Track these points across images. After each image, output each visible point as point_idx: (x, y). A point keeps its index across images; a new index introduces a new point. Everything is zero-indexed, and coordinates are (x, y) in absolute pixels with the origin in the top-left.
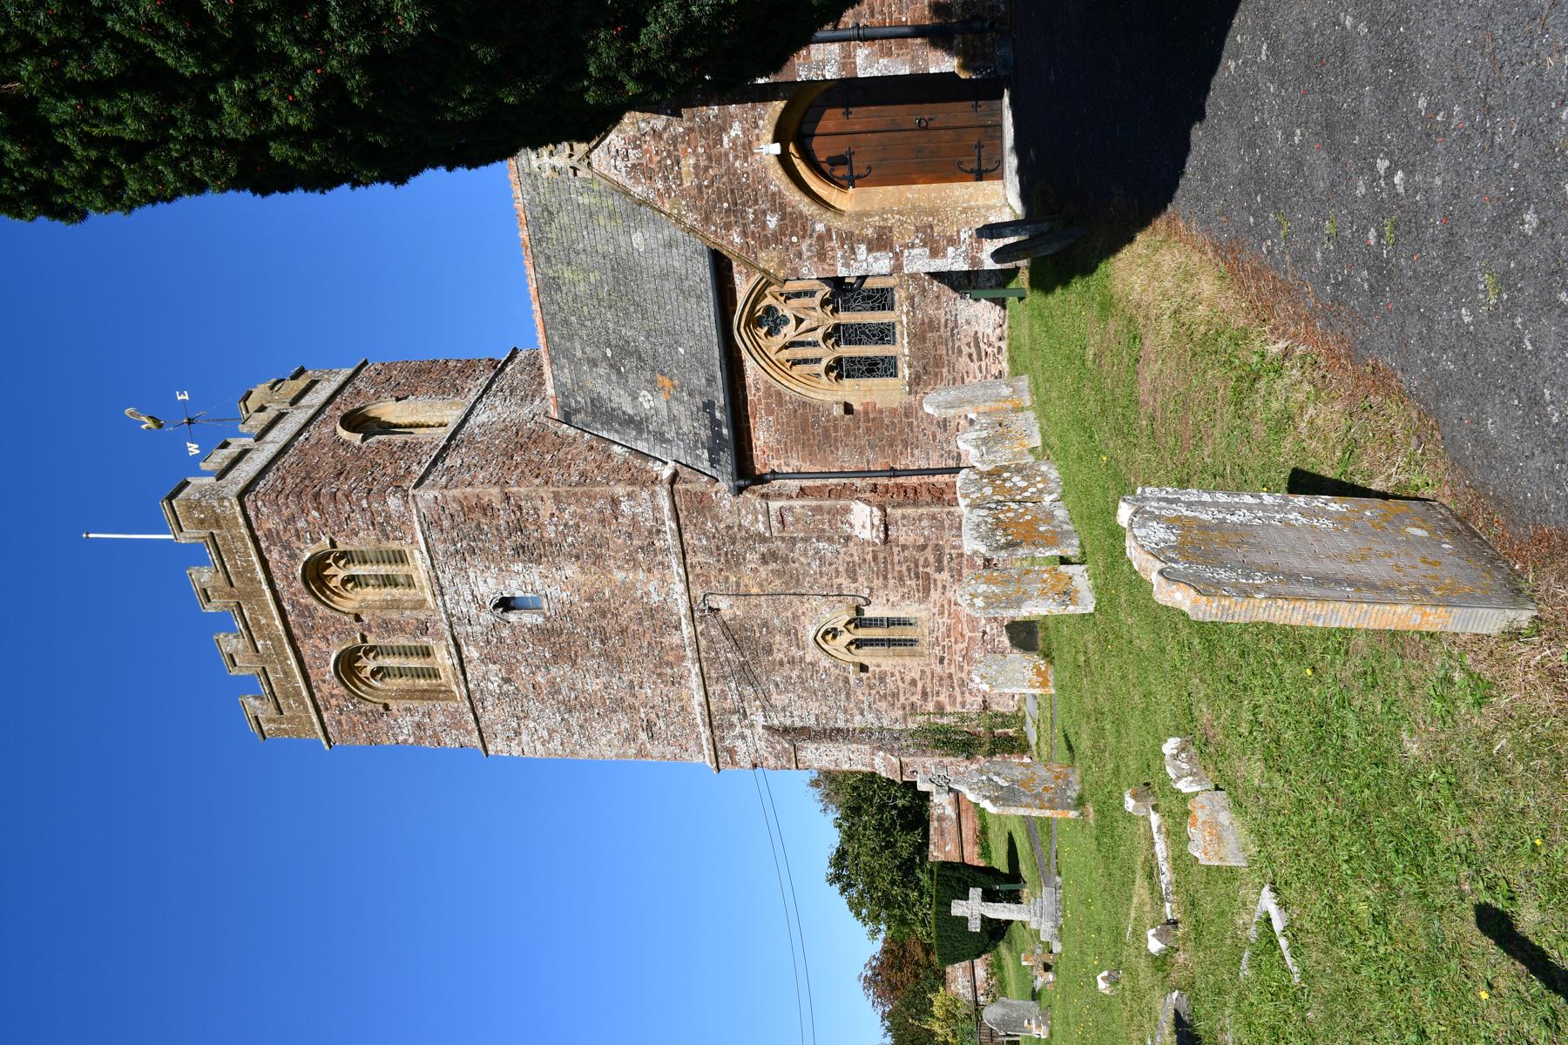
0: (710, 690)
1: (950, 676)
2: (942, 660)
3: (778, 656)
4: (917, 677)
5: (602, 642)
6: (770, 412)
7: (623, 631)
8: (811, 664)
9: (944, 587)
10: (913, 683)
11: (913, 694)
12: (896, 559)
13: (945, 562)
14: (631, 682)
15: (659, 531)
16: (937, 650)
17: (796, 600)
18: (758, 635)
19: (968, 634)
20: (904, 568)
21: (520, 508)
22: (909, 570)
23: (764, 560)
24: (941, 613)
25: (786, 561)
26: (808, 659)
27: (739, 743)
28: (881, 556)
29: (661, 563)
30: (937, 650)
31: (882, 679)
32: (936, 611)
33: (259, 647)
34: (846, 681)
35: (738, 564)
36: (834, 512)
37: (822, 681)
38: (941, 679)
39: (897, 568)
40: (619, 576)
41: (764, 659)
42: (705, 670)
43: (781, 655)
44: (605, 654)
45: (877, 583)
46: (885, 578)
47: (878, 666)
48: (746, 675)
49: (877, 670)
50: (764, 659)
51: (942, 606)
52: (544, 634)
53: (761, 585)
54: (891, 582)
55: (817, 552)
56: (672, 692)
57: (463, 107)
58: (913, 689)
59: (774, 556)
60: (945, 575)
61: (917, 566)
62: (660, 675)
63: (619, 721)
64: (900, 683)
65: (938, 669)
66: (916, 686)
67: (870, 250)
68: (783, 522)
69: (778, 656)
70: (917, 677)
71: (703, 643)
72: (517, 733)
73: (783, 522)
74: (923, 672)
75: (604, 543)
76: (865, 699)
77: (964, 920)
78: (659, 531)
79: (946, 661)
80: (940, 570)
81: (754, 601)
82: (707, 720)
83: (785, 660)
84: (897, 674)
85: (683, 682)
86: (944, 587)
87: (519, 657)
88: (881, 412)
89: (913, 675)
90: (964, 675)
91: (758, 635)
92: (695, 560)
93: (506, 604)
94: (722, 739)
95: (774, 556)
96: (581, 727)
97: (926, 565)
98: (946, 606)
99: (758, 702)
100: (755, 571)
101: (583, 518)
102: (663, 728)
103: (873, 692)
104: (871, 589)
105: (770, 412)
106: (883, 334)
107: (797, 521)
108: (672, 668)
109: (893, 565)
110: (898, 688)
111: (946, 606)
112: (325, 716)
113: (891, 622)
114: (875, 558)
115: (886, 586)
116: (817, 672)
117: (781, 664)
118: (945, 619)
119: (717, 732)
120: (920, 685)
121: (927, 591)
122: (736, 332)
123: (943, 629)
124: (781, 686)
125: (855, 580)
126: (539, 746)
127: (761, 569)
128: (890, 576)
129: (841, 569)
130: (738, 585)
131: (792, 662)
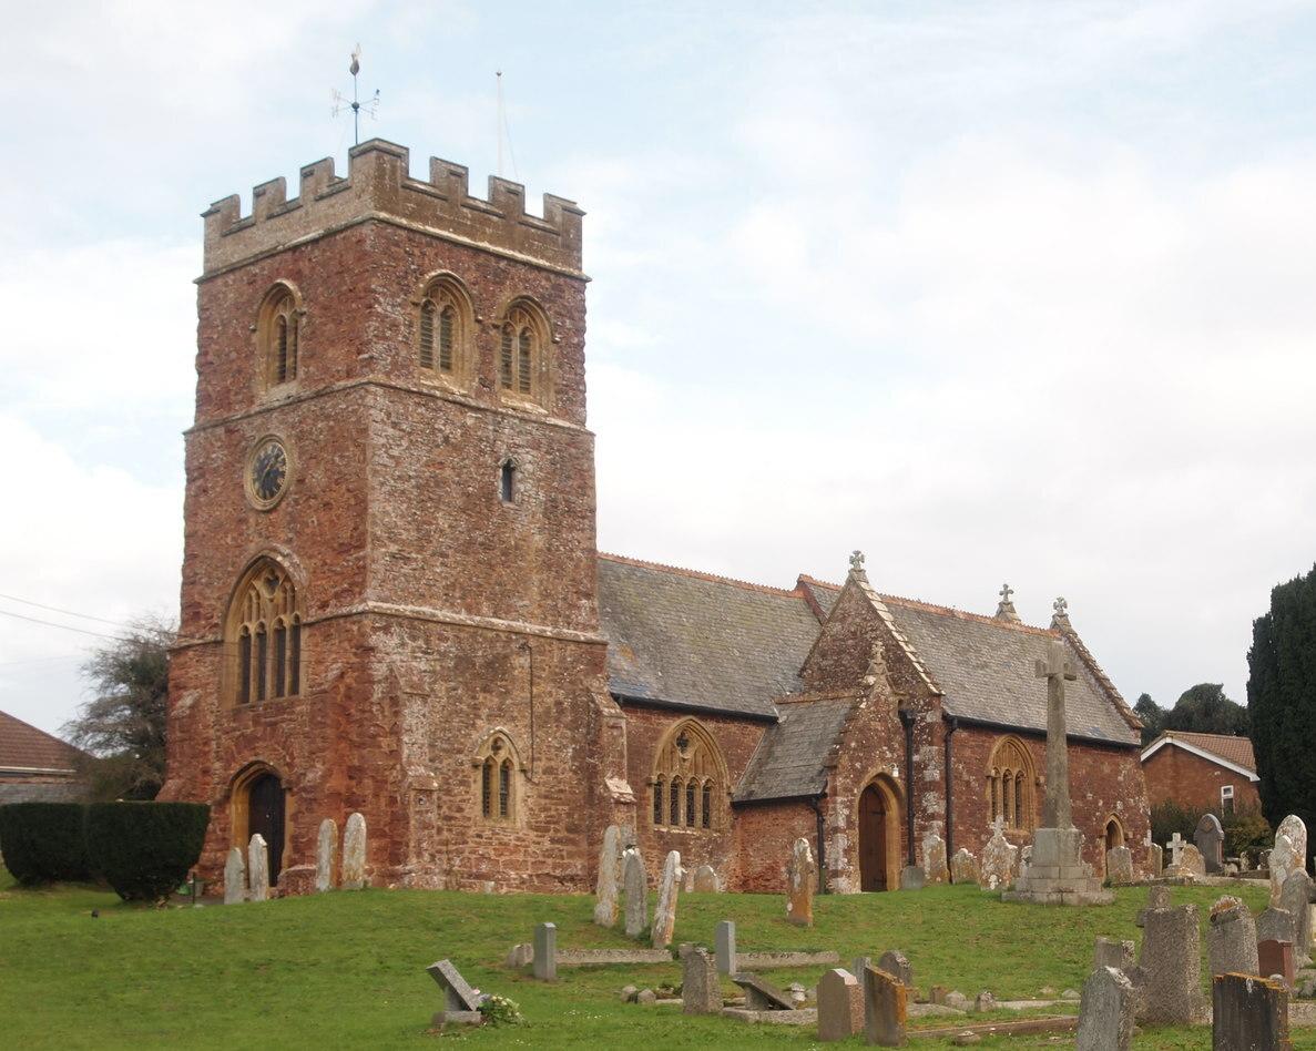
0: (448, 628)
1: (465, 842)
2: (479, 836)
3: (481, 696)
4: (465, 814)
5: (481, 544)
6: (646, 730)
7: (492, 567)
8: (474, 724)
9: (539, 843)
10: (460, 810)
11: (449, 808)
12: (560, 807)
13: (557, 846)
14: (447, 556)
15: (569, 624)
16: (488, 833)
17: (527, 722)
18: (499, 683)
19: (502, 859)
20: (553, 813)
21: (583, 518)
22: (551, 817)
23: (559, 703)
24: (518, 839)
25: (557, 720)
26: (479, 722)
27: (396, 640)
28: (562, 796)
29: (546, 618)
30: (488, 833)
31: (462, 783)
32: (521, 835)
33: (465, 210)
34: (460, 751)
35: (554, 681)
36: (619, 766)
37: (459, 731)
38: (463, 834)
39: (553, 808)
40: (535, 578)
41: (478, 684)
42: (467, 629)
43: (481, 699)
44: (471, 543)
45: (543, 790)
46: (546, 797)
47: (475, 781)
48: (464, 662)
49: (471, 780)
50: (478, 684)
51: (524, 841)
52: (489, 496)
53: (539, 696)
54: (543, 801)
55: (565, 747)
56: (439, 589)
57: (43, 737)
58: (454, 808)
59: (561, 712)
60: (547, 845)
61: (554, 823)
62: (453, 585)
63: (408, 530)
64: (459, 798)
65: (471, 832)
66: (457, 811)
67: (847, 816)
68: (613, 727)
69: (481, 696)
70: (465, 814)
71: (490, 635)
72: (395, 425)
73: (613, 727)
74: (469, 819)
75: (559, 576)
76: (444, 764)
77: (1171, 840)
78: (569, 624)
79: (478, 840)
80: (553, 841)
81: (527, 686)
82: (422, 617)
83: (477, 702)
84: (468, 797)
85: (448, 604)
86: (539, 843)
87: (467, 461)
88: (645, 809)
89: (467, 810)
90: (466, 854)
91: (499, 683)
92: (555, 647)
93: (509, 470)
94: (401, 625)
95: (561, 712)
96: (403, 492)
97: (556, 831)
98: (523, 844)
99: (438, 668)
100: (550, 694)
101: (577, 566)
102: (403, 570)
103: (450, 773)
104: (537, 785)
105: (646, 730)
106: (674, 821)
107: (614, 738)
108: (460, 598)
109: (556, 804)
110: (455, 795)
111: (523, 844)
112: (404, 233)
113: (505, 797)
114: (561, 791)
115: (539, 796)
116: (467, 728)
117: (474, 698)
118: (513, 842)
119: (406, 622)
120: (458, 815)
121: (537, 829)
122: (694, 719)
123: (506, 839)
124: (453, 693)
125: (544, 773)
126: (383, 441)
127: (552, 699)
128: (547, 801)
129: (553, 763)
130: (540, 677)
131: (476, 708)
